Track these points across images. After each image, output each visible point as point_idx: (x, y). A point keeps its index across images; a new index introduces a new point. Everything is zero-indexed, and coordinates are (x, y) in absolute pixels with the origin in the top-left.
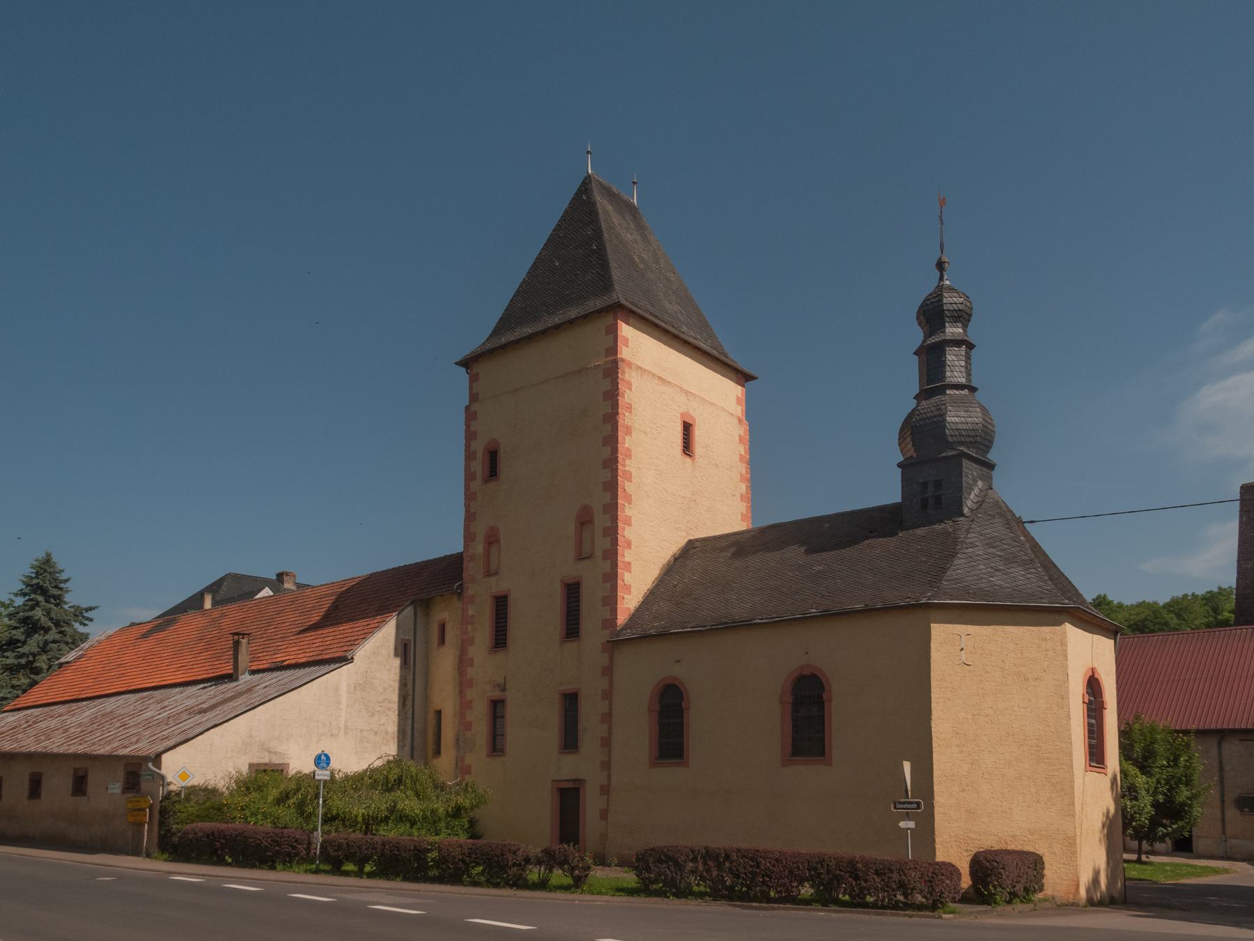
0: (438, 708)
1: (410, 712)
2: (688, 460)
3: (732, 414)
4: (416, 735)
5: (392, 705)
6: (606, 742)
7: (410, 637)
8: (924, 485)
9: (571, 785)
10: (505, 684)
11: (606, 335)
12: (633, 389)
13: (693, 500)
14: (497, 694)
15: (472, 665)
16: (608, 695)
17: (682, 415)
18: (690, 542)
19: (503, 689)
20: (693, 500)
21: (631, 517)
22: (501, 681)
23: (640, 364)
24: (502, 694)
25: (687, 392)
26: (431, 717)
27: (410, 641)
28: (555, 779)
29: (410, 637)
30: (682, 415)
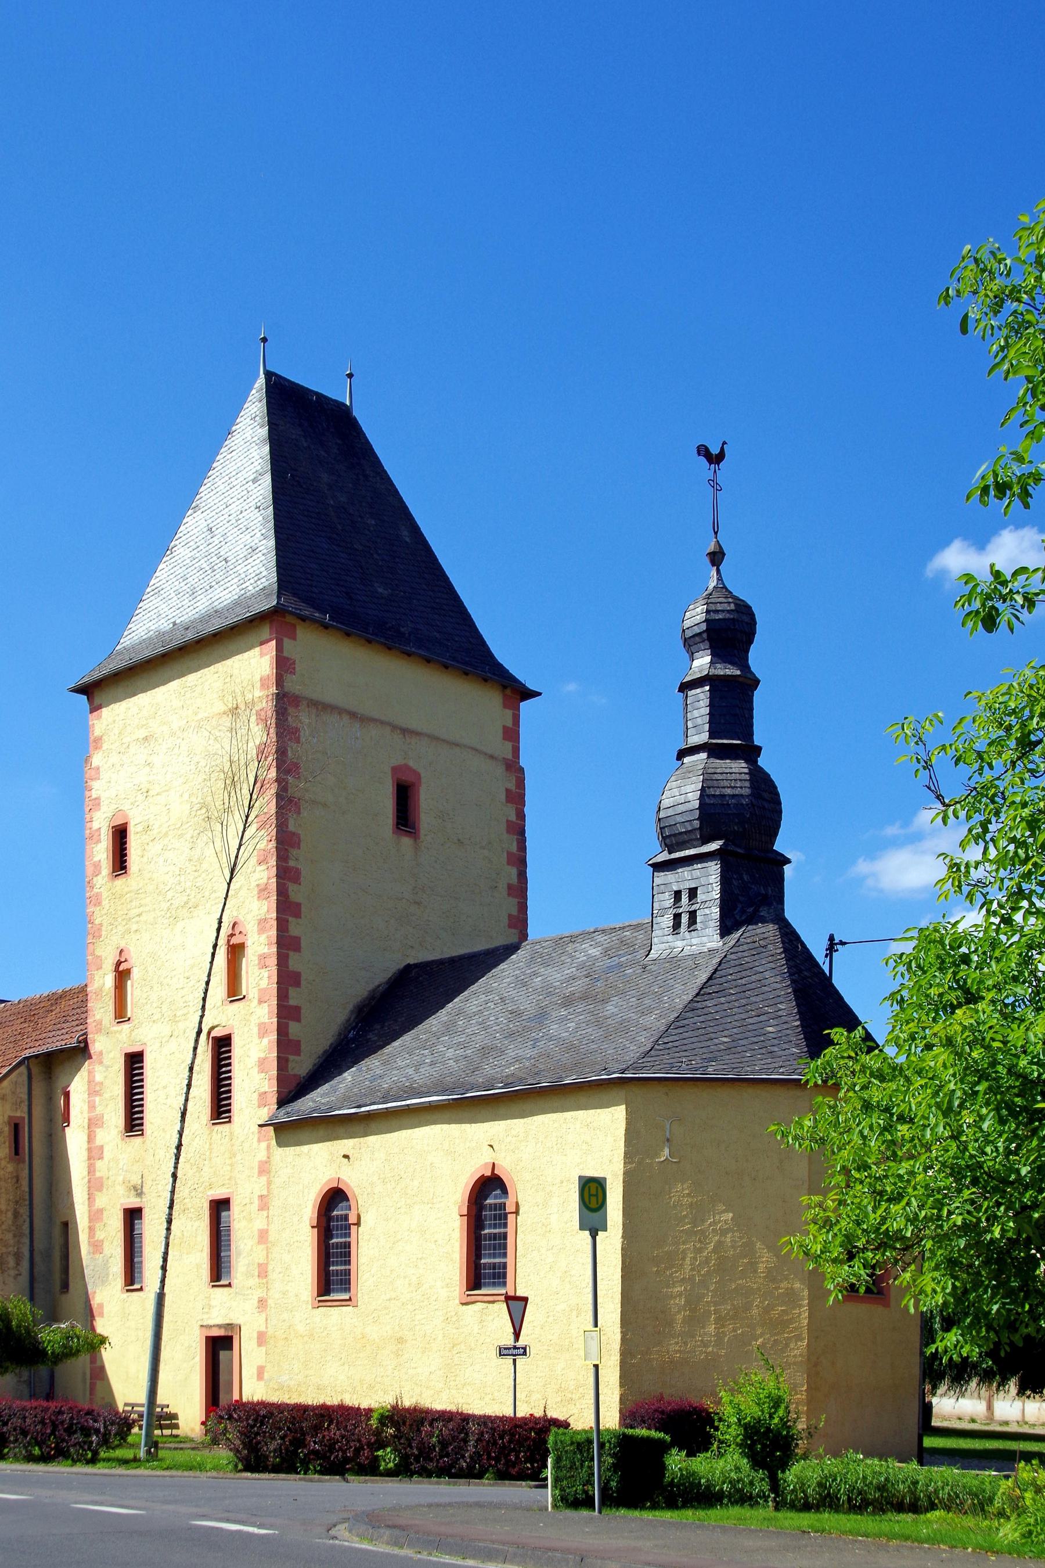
0: (64, 1220)
1: (27, 1225)
2: (406, 841)
3: (492, 757)
4: (38, 1259)
5: (573, 1186)
6: (263, 1272)
7: (22, 1113)
8: (678, 895)
9: (220, 1333)
10: (142, 1187)
11: (261, 657)
12: (303, 739)
13: (415, 903)
14: (133, 1202)
15: (101, 1158)
16: (264, 1202)
17: (395, 770)
18: (408, 968)
19: (139, 1192)
20: (415, 903)
21: (300, 938)
22: (136, 1180)
23: (315, 696)
24: (138, 1200)
25: (405, 731)
26: (57, 1231)
27: (24, 1118)
28: (205, 1324)
29: (22, 1113)
30: (395, 770)
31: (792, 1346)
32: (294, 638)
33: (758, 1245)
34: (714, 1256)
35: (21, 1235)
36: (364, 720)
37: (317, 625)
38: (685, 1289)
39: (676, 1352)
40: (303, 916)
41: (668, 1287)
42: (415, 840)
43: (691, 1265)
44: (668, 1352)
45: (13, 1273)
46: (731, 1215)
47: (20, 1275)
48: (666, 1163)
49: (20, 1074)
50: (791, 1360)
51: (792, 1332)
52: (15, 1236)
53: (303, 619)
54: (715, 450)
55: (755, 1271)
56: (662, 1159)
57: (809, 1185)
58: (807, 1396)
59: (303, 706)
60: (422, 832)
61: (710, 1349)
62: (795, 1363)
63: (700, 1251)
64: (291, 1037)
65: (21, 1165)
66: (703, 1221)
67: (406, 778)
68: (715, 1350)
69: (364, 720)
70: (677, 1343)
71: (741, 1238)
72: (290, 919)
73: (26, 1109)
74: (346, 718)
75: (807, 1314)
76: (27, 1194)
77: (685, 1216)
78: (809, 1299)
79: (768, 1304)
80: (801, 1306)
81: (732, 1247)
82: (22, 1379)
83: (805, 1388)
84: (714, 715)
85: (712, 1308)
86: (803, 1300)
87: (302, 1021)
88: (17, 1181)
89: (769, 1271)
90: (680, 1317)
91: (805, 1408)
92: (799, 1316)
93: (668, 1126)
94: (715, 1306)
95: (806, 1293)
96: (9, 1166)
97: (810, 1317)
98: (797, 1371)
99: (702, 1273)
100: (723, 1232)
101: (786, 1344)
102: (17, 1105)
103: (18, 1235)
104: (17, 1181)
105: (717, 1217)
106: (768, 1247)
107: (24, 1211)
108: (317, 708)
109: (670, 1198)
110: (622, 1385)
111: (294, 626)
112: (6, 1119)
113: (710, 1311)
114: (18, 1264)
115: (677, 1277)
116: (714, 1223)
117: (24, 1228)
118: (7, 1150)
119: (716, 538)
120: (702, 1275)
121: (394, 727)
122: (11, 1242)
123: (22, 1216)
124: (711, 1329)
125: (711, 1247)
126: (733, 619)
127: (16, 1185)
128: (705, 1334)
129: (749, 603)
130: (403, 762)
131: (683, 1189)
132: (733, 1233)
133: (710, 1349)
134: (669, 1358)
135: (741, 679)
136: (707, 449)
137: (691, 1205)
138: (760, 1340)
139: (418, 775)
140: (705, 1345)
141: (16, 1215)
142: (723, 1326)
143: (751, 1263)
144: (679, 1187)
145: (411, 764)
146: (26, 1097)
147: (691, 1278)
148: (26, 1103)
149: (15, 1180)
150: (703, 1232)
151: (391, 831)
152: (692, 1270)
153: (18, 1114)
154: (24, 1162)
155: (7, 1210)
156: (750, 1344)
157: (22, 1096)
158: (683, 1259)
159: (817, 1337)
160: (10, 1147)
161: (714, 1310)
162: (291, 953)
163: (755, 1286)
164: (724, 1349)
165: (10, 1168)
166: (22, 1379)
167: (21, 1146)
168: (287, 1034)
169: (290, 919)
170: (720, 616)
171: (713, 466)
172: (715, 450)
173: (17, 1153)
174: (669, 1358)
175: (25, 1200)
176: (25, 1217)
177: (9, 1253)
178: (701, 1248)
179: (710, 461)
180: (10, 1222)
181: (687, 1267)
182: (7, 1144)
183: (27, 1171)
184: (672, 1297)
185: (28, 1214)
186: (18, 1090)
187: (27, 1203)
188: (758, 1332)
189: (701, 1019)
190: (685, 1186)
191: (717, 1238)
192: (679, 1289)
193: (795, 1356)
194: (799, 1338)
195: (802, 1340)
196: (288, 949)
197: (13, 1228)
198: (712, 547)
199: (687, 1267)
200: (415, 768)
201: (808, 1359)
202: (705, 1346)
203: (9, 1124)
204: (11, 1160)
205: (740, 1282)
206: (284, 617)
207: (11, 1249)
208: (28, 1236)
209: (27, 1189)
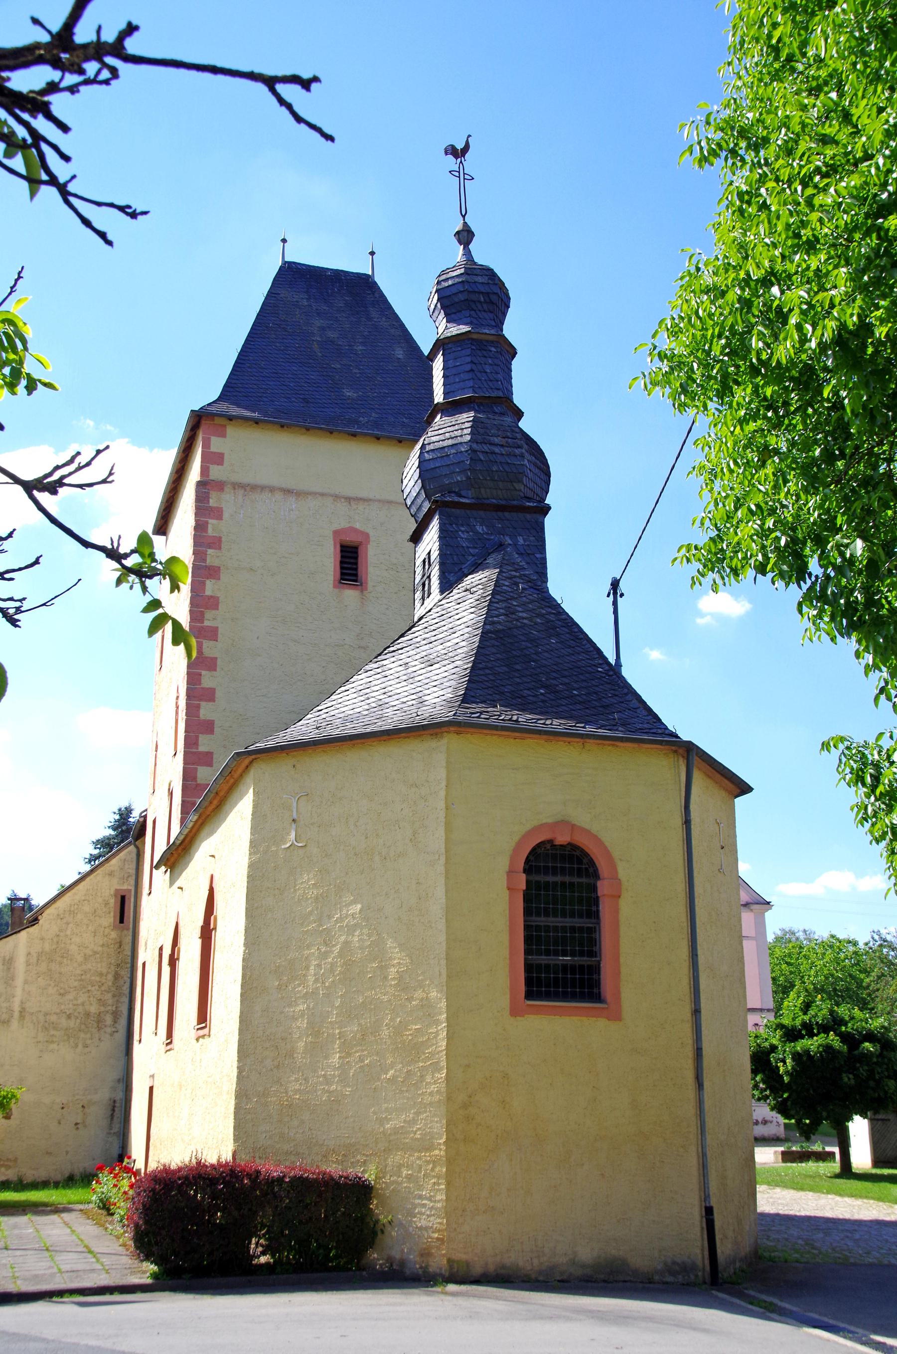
1: (128, 985)
21: (214, 689)
25: (349, 499)
29: (129, 886)
31: (428, 1079)
32: (224, 435)
33: (389, 943)
34: (340, 962)
35: (120, 995)
36: (299, 494)
37: (251, 423)
38: (308, 1008)
39: (296, 1091)
40: (218, 669)
41: (290, 1005)
42: (362, 591)
43: (315, 975)
44: (286, 1092)
45: (109, 1030)
46: (359, 906)
47: (117, 1032)
48: (292, 848)
49: (130, 853)
50: (428, 1099)
51: (428, 1058)
52: (114, 996)
53: (231, 418)
54: (460, 146)
55: (386, 978)
56: (288, 845)
57: (447, 859)
58: (446, 1151)
59: (228, 489)
60: (370, 584)
61: (334, 1087)
62: (431, 1104)
63: (325, 955)
64: (199, 781)
65: (125, 932)
66: (330, 917)
67: (350, 539)
68: (339, 1088)
69: (299, 494)
70: (297, 1080)
71: (369, 935)
72: (203, 673)
73: (133, 882)
74: (279, 496)
75: (445, 1033)
76: (130, 958)
77: (311, 913)
78: (447, 1012)
79: (400, 1022)
80: (437, 1023)
81: (361, 948)
82: (112, 1131)
83: (444, 1139)
84: (448, 377)
85: (337, 1031)
86: (440, 1014)
87: (214, 765)
88: (120, 946)
89: (400, 977)
90: (301, 1044)
91: (444, 1170)
92: (435, 1037)
93: (295, 804)
94: (340, 1028)
95: (443, 1004)
96: (112, 933)
97: (449, 1038)
98: (435, 1115)
99: (327, 984)
100: (351, 929)
101: (422, 1076)
102: (123, 879)
103: (117, 996)
104: (120, 946)
105: (344, 912)
106: (400, 945)
107: (125, 973)
108: (245, 490)
109: (295, 891)
110: (236, 1140)
111: (225, 426)
112: (112, 892)
113: (334, 1034)
114: (115, 1022)
115: (299, 992)
116: (341, 919)
117: (124, 988)
118: (112, 920)
119: (464, 220)
120: (328, 988)
121: (336, 497)
122: (110, 1002)
123: (122, 977)
124: (335, 1059)
125: (337, 949)
126: (463, 282)
127: (119, 950)
128: (329, 1066)
129: (492, 267)
130: (348, 525)
131: (309, 880)
132: (362, 929)
133: (334, 1087)
134: (287, 1100)
135: (475, 336)
136: (453, 147)
137: (317, 899)
138: (391, 1072)
139: (367, 536)
140: (327, 1080)
141: (117, 976)
142: (349, 1054)
143: (381, 968)
144: (305, 877)
145: (357, 526)
146: (134, 872)
147: (315, 993)
148: (134, 877)
149: (118, 944)
150: (328, 930)
151: (331, 586)
152: (316, 981)
153: (125, 887)
154: (128, 929)
155: (108, 973)
156: (379, 1079)
157: (130, 871)
158: (307, 968)
159: (468, 1066)
160: (114, 917)
161: (339, 1033)
162: (203, 704)
163: (385, 998)
164: (349, 1086)
165: (114, 935)
166: (112, 1131)
167: (126, 914)
168: (195, 778)
169: (203, 673)
170: (450, 282)
171: (459, 160)
172: (460, 146)
173: (122, 921)
174: (287, 1100)
175: (126, 963)
176: (125, 978)
177: (108, 1012)
178: (326, 952)
179: (456, 157)
180: (110, 984)
181: (311, 979)
182: (112, 914)
183: (130, 938)
184: (295, 1019)
185: (129, 976)
186: (127, 866)
187: (129, 965)
188: (389, 1062)
189: (413, 686)
190: (311, 876)
191: (343, 938)
192: (301, 1007)
193: (431, 1094)
194: (436, 1068)
195: (439, 1070)
196: (201, 700)
197: (113, 989)
198: (459, 227)
199: (311, 979)
200: (362, 529)
201: (449, 1098)
202: (327, 1084)
203: (116, 896)
204: (115, 928)
205: (368, 993)
206: (213, 420)
207: (110, 1008)
208: (128, 995)
209: (129, 953)
